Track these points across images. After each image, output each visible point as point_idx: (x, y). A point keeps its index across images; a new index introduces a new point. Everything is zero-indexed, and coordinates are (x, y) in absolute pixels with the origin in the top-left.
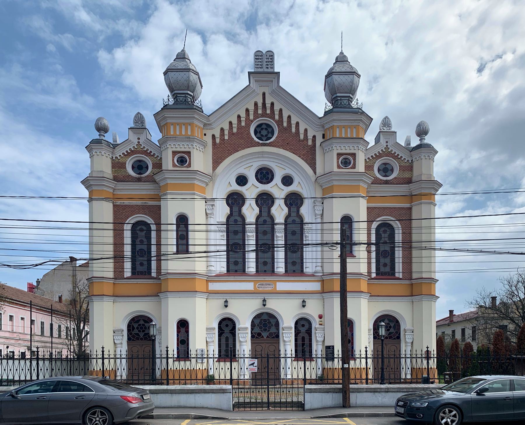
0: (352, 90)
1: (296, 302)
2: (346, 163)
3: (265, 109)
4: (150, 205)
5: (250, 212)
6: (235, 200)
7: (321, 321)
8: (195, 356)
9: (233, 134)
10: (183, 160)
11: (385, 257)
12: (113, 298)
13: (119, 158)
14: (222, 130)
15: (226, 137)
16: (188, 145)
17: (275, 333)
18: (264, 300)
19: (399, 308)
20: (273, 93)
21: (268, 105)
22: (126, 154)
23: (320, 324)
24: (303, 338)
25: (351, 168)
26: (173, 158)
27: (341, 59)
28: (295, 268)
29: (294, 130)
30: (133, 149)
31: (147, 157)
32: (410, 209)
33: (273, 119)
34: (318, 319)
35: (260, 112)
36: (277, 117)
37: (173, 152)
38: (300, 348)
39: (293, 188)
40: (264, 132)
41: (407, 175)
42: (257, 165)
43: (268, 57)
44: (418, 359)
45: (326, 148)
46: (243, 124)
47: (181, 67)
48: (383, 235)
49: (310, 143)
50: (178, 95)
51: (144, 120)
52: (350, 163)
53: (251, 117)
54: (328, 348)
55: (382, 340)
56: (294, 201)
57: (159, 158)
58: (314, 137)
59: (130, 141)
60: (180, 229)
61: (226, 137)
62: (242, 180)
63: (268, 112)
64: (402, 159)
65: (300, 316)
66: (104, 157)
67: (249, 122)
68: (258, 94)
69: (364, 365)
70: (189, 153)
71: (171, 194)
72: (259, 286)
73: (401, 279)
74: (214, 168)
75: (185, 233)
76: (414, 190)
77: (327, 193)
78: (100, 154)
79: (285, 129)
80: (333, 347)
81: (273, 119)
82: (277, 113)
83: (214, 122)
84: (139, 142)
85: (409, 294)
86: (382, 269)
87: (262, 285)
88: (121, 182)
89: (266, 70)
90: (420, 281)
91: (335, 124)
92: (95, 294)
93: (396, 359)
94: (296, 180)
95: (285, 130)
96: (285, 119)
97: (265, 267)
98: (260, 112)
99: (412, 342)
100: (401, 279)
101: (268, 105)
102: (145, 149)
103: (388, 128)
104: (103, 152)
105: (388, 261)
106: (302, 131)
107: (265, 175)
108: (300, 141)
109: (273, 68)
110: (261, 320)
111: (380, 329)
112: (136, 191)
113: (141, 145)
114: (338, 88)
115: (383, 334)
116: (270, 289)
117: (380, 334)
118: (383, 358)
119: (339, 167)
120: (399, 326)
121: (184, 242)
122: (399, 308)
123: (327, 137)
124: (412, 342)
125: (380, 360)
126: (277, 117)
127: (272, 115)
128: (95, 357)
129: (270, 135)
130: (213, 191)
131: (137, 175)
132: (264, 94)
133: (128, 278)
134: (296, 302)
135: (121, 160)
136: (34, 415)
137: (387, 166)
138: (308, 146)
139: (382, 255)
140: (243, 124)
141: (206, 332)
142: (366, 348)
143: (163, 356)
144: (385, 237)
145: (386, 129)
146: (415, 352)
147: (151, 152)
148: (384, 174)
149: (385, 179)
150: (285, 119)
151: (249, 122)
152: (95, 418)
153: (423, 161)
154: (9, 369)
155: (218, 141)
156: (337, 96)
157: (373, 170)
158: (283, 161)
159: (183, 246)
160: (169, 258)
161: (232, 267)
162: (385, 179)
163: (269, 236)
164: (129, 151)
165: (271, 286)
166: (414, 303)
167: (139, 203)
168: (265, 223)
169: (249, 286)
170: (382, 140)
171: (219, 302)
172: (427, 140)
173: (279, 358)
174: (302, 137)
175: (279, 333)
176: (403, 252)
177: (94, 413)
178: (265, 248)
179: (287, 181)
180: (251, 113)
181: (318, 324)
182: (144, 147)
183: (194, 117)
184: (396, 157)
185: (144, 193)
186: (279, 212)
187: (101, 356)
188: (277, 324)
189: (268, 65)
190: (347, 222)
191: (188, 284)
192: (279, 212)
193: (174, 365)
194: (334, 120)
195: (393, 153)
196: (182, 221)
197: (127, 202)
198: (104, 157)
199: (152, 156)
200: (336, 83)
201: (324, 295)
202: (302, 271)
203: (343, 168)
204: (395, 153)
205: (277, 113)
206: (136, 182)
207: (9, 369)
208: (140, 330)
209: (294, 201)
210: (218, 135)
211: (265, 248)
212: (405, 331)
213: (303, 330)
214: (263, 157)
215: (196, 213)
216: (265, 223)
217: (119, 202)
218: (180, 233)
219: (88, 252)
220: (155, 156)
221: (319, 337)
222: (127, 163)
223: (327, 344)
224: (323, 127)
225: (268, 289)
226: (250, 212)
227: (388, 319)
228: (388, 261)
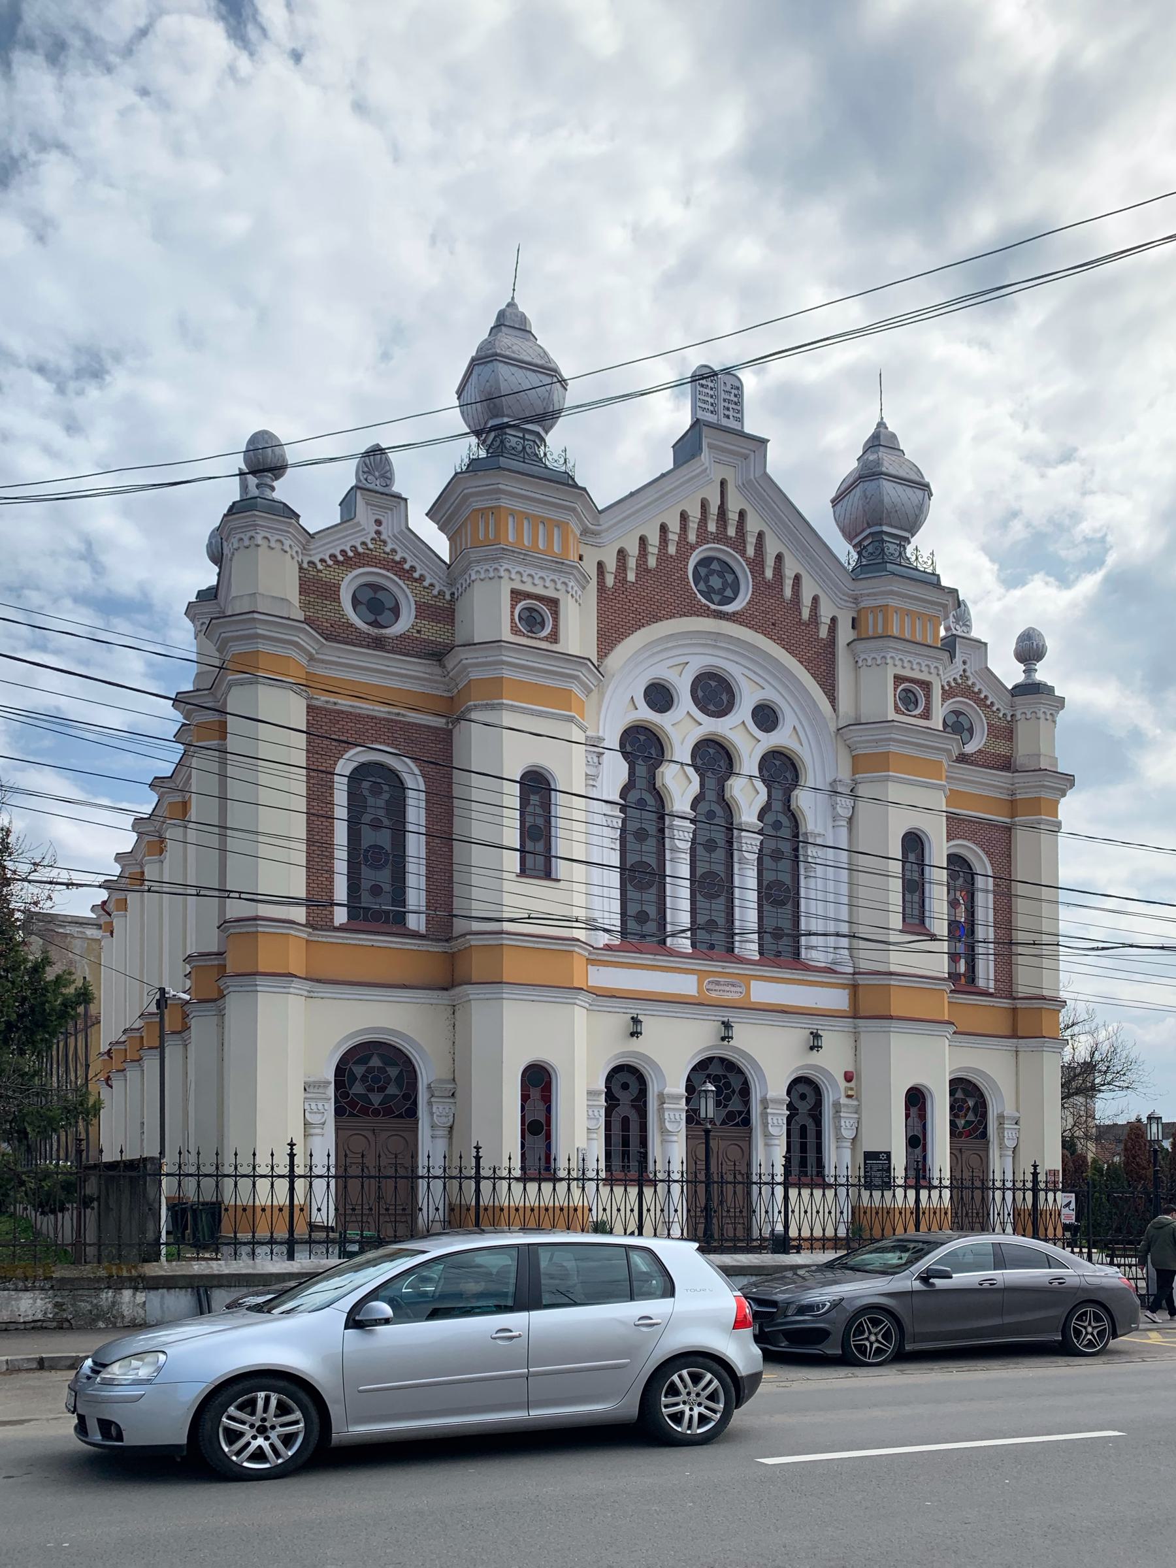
0: (913, 523)
1: (794, 1036)
2: (908, 700)
3: (721, 523)
4: (409, 723)
5: (680, 786)
6: (642, 746)
7: (851, 1089)
8: (267, 1171)
9: (648, 571)
10: (536, 615)
11: (376, 867)
12: (308, 985)
13: (320, 567)
14: (622, 554)
15: (631, 577)
16: (542, 578)
17: (740, 1113)
18: (727, 1025)
19: (990, 1063)
20: (746, 487)
21: (733, 517)
22: (341, 558)
23: (849, 1097)
24: (625, 1122)
25: (545, 639)
26: (513, 607)
27: (509, 321)
28: (783, 945)
29: (788, 592)
30: (360, 550)
31: (401, 582)
32: (1008, 829)
33: (743, 553)
34: (842, 1084)
35: (712, 527)
36: (750, 551)
37: (514, 592)
38: (617, 1148)
39: (778, 738)
40: (717, 582)
41: (1002, 749)
42: (698, 663)
43: (728, 388)
44: (764, 1188)
45: (863, 656)
46: (672, 550)
47: (528, 359)
48: (371, 801)
49: (823, 633)
50: (886, 538)
51: (391, 471)
52: (543, 625)
53: (692, 537)
54: (869, 1156)
55: (707, 1132)
56: (781, 770)
57: (435, 592)
58: (834, 620)
59: (358, 524)
60: (529, 809)
61: (631, 577)
62: (659, 696)
63: (731, 532)
64: (994, 709)
65: (799, 1073)
66: (288, 556)
67: (686, 548)
68: (711, 481)
69: (282, 1198)
70: (553, 603)
71: (512, 708)
72: (710, 987)
73: (991, 995)
74: (603, 653)
75: (540, 821)
76: (1020, 788)
77: (869, 763)
78: (278, 546)
79: (768, 585)
80: (888, 1154)
81: (743, 553)
82: (751, 540)
83: (606, 530)
84: (378, 533)
85: (1008, 1033)
86: (366, 900)
87: (718, 983)
88: (347, 643)
89: (725, 422)
90: (1036, 1004)
91: (894, 602)
92: (261, 970)
93: (366, 1181)
94: (789, 718)
95: (768, 589)
96: (770, 562)
97: (714, 936)
98: (712, 527)
99: (451, 1127)
100: (991, 995)
101: (733, 517)
102: (397, 558)
103: (964, 628)
104: (287, 543)
105: (384, 877)
106: (807, 601)
107: (714, 693)
108: (800, 622)
109: (740, 420)
110: (725, 1077)
111: (703, 1101)
112: (384, 679)
113: (385, 542)
114: (889, 513)
115: (711, 1115)
116: (736, 996)
117: (703, 1115)
118: (708, 1184)
119: (515, 631)
120: (984, 1104)
121: (540, 847)
122: (990, 1063)
123: (871, 625)
124: (451, 1127)
125: (701, 1188)
126: (750, 551)
127: (741, 548)
128: (231, 1171)
129: (729, 593)
130: (599, 714)
131: (366, 626)
132: (723, 483)
133: (341, 929)
134: (794, 1036)
135: (326, 575)
136: (996, 1321)
137: (961, 718)
138: (818, 639)
139: (366, 860)
140: (672, 550)
141: (586, 1102)
142: (292, 1145)
143: (278, 1171)
144: (377, 805)
145: (376, 484)
146: (456, 1162)
147: (413, 568)
148: (371, 618)
149: (374, 631)
150: (770, 562)
151: (686, 548)
152: (876, 1334)
153: (1042, 721)
154: (672, 1210)
155: (610, 581)
156: (882, 532)
157: (337, 600)
158: (762, 669)
159: (538, 855)
160: (1045, 952)
161: (632, 925)
162: (374, 631)
163: (651, 844)
164: (351, 554)
165: (739, 989)
166: (1021, 1055)
167: (381, 711)
168: (714, 810)
169: (686, 985)
170: (364, 515)
171: (615, 1021)
172: (1043, 673)
173: (984, 1188)
174: (806, 614)
175: (748, 1112)
176: (995, 931)
177: (1098, 1318)
178: (713, 886)
179: (766, 717)
180: (693, 526)
181: (843, 1094)
182: (394, 551)
183: (574, 510)
184: (982, 702)
185: (375, 680)
186: (748, 796)
187: (286, 1171)
188: (745, 1091)
189: (728, 409)
190: (914, 842)
191: (552, 968)
192: (748, 796)
193: (515, 1195)
194: (892, 593)
195: (976, 690)
196: (537, 786)
197: (344, 703)
198: (288, 556)
199: (416, 580)
200: (886, 499)
201: (860, 1022)
202: (798, 954)
203: (903, 714)
204: (980, 691)
205: (751, 540)
206: (368, 647)
207: (821, 1214)
208: (374, 1089)
209: (781, 770)
210: (611, 566)
211: (713, 886)
212: (1001, 1118)
213: (803, 1107)
214: (715, 646)
215: (570, 770)
216: (714, 810)
217: (322, 699)
218: (530, 820)
219: (474, 870)
220: (426, 584)
221: (846, 1129)
222: (343, 585)
223: (871, 1144)
224: (856, 600)
225: (730, 996)
226: (680, 786)
227: (381, 1056)
228: (384, 877)
